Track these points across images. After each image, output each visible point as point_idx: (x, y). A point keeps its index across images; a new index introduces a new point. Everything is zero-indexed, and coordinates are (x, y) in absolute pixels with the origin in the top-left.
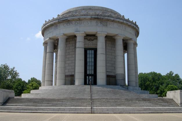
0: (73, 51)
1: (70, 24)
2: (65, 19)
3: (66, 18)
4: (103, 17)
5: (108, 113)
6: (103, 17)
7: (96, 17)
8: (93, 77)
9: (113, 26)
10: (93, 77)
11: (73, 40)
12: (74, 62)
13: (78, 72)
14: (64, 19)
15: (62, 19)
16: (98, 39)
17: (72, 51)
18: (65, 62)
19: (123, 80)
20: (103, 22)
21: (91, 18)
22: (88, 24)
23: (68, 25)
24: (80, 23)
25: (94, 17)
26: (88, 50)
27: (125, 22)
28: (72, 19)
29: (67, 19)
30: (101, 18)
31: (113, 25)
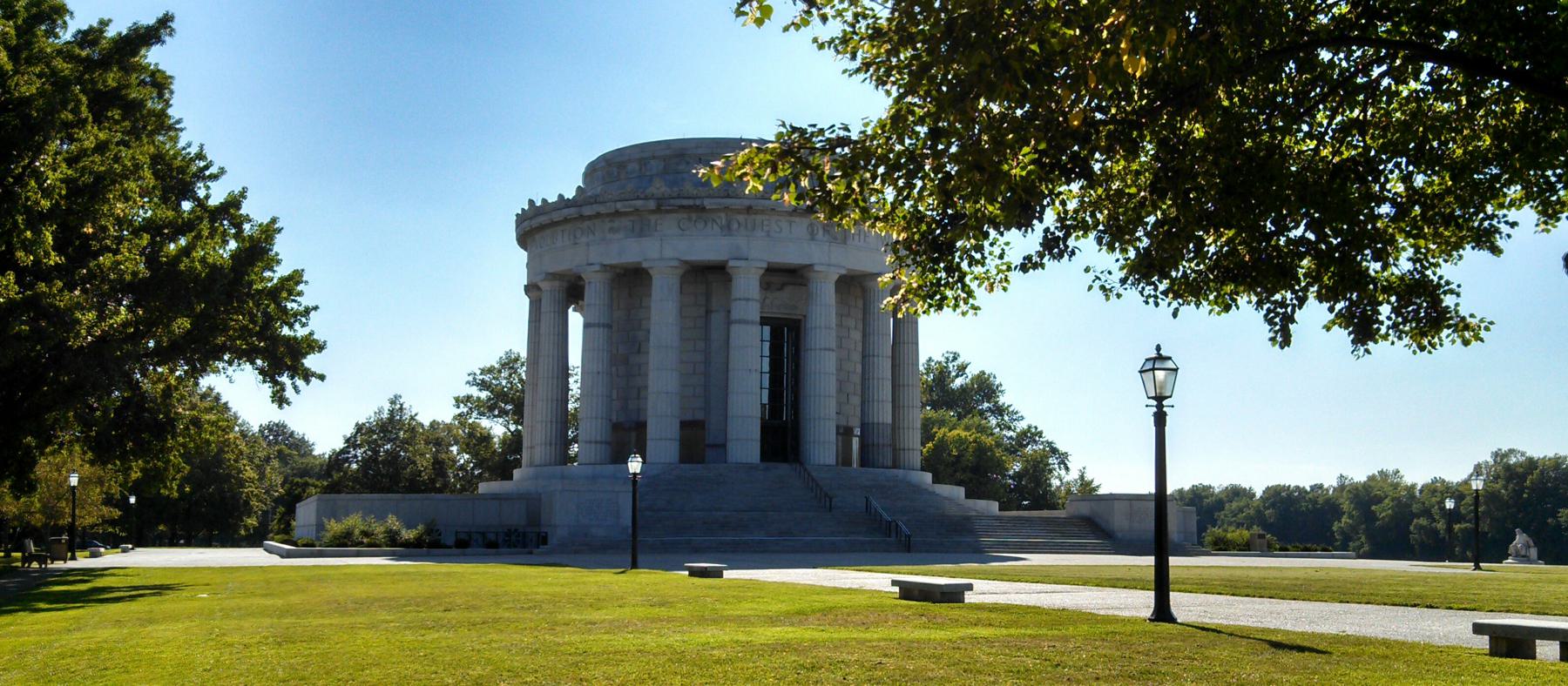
1: (709, 225)
2: (691, 202)
9: (865, 241)
14: (685, 202)
23: (701, 225)
29: (698, 202)
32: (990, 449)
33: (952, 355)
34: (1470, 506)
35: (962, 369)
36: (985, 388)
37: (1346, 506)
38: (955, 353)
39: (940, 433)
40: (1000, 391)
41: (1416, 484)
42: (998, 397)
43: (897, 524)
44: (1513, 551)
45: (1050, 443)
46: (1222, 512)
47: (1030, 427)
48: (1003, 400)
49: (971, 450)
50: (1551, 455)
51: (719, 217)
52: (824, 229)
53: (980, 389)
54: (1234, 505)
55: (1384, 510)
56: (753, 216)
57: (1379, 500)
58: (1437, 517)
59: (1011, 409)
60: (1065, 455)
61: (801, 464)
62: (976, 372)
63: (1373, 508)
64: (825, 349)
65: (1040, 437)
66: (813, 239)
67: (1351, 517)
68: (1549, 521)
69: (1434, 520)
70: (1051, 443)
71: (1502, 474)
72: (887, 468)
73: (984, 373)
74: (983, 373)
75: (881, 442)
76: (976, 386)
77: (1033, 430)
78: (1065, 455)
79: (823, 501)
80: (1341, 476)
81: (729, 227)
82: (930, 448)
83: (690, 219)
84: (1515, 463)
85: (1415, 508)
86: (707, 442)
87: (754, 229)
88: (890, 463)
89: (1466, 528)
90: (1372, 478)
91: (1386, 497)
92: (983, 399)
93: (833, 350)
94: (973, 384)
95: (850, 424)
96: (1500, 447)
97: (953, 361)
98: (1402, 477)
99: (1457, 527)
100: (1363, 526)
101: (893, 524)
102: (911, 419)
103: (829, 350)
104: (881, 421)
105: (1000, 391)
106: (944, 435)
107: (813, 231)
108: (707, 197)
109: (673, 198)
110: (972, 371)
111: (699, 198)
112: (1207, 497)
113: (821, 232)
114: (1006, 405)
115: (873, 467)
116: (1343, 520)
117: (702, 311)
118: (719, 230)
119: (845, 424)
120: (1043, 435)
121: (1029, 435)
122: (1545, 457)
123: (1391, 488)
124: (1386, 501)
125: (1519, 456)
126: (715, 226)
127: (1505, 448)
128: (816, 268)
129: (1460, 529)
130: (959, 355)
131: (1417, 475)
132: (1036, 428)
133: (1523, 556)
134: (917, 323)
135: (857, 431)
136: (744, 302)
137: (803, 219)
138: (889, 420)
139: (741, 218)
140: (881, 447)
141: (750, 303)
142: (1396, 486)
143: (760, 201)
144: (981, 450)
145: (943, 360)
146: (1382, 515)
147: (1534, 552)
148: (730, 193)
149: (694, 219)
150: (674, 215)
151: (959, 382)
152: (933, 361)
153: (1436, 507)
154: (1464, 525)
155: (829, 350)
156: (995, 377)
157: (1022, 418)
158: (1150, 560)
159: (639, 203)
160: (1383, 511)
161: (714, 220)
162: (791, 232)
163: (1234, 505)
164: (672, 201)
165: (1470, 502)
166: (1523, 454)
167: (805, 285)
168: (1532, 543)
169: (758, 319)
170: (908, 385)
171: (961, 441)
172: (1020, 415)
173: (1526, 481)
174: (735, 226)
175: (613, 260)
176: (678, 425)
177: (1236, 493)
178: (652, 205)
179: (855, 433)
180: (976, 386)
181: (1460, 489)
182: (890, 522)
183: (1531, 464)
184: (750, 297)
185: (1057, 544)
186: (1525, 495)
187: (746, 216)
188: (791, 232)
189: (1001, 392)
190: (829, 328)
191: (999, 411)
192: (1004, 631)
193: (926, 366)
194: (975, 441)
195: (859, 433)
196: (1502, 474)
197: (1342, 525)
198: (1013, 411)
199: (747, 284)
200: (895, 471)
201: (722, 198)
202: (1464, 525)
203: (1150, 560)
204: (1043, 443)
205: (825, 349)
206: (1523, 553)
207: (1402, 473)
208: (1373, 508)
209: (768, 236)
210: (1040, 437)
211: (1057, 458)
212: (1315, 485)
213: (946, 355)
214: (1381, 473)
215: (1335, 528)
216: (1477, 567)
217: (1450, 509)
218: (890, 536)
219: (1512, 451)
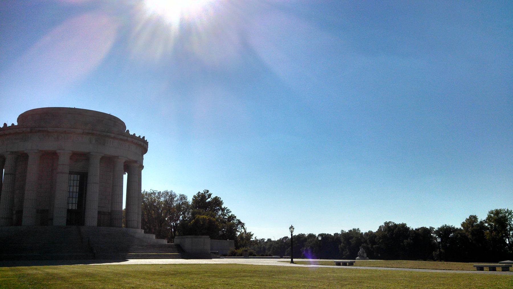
29: (46, 129)
32: (214, 222)
33: (206, 191)
34: (378, 239)
35: (210, 195)
36: (217, 202)
37: (342, 240)
38: (207, 190)
39: (197, 216)
41: (363, 233)
44: (359, 255)
45: (239, 220)
46: (306, 242)
49: (207, 222)
50: (401, 223)
53: (216, 202)
54: (309, 240)
55: (353, 241)
57: (352, 238)
58: (368, 243)
59: (227, 209)
60: (244, 224)
63: (350, 240)
65: (235, 218)
67: (344, 243)
68: (401, 244)
69: (368, 244)
70: (239, 220)
71: (387, 229)
74: (217, 197)
78: (244, 224)
80: (342, 230)
82: (193, 221)
84: (391, 226)
85: (362, 241)
89: (377, 247)
90: (350, 231)
91: (354, 237)
93: (97, 183)
96: (386, 221)
97: (207, 193)
98: (360, 230)
99: (374, 246)
100: (348, 246)
106: (199, 217)
110: (213, 196)
112: (302, 238)
114: (225, 208)
116: (341, 244)
120: (236, 218)
122: (400, 224)
123: (355, 234)
124: (354, 238)
125: (392, 223)
127: (388, 221)
129: (375, 247)
130: (209, 191)
131: (364, 230)
132: (234, 215)
133: (362, 256)
142: (357, 233)
144: (210, 222)
145: (203, 192)
146: (353, 243)
147: (365, 255)
151: (209, 200)
152: (200, 193)
153: (368, 240)
154: (376, 246)
156: (220, 198)
157: (231, 212)
158: (290, 259)
159: (24, 129)
160: (353, 241)
163: (309, 240)
165: (378, 238)
166: (394, 223)
168: (364, 251)
169: (68, 172)
171: (204, 219)
172: (230, 211)
173: (394, 231)
175: (15, 150)
177: (311, 236)
178: (29, 130)
181: (375, 234)
183: (396, 226)
185: (159, 255)
186: (394, 236)
192: (508, 264)
193: (198, 195)
194: (208, 219)
196: (387, 229)
197: (341, 246)
198: (228, 209)
199: (64, 160)
202: (376, 246)
203: (290, 259)
204: (236, 220)
206: (362, 255)
207: (360, 229)
208: (350, 240)
210: (235, 218)
211: (241, 225)
212: (336, 233)
213: (205, 191)
214: (354, 229)
215: (339, 247)
216: (292, 262)
217: (320, 240)
219: (390, 222)
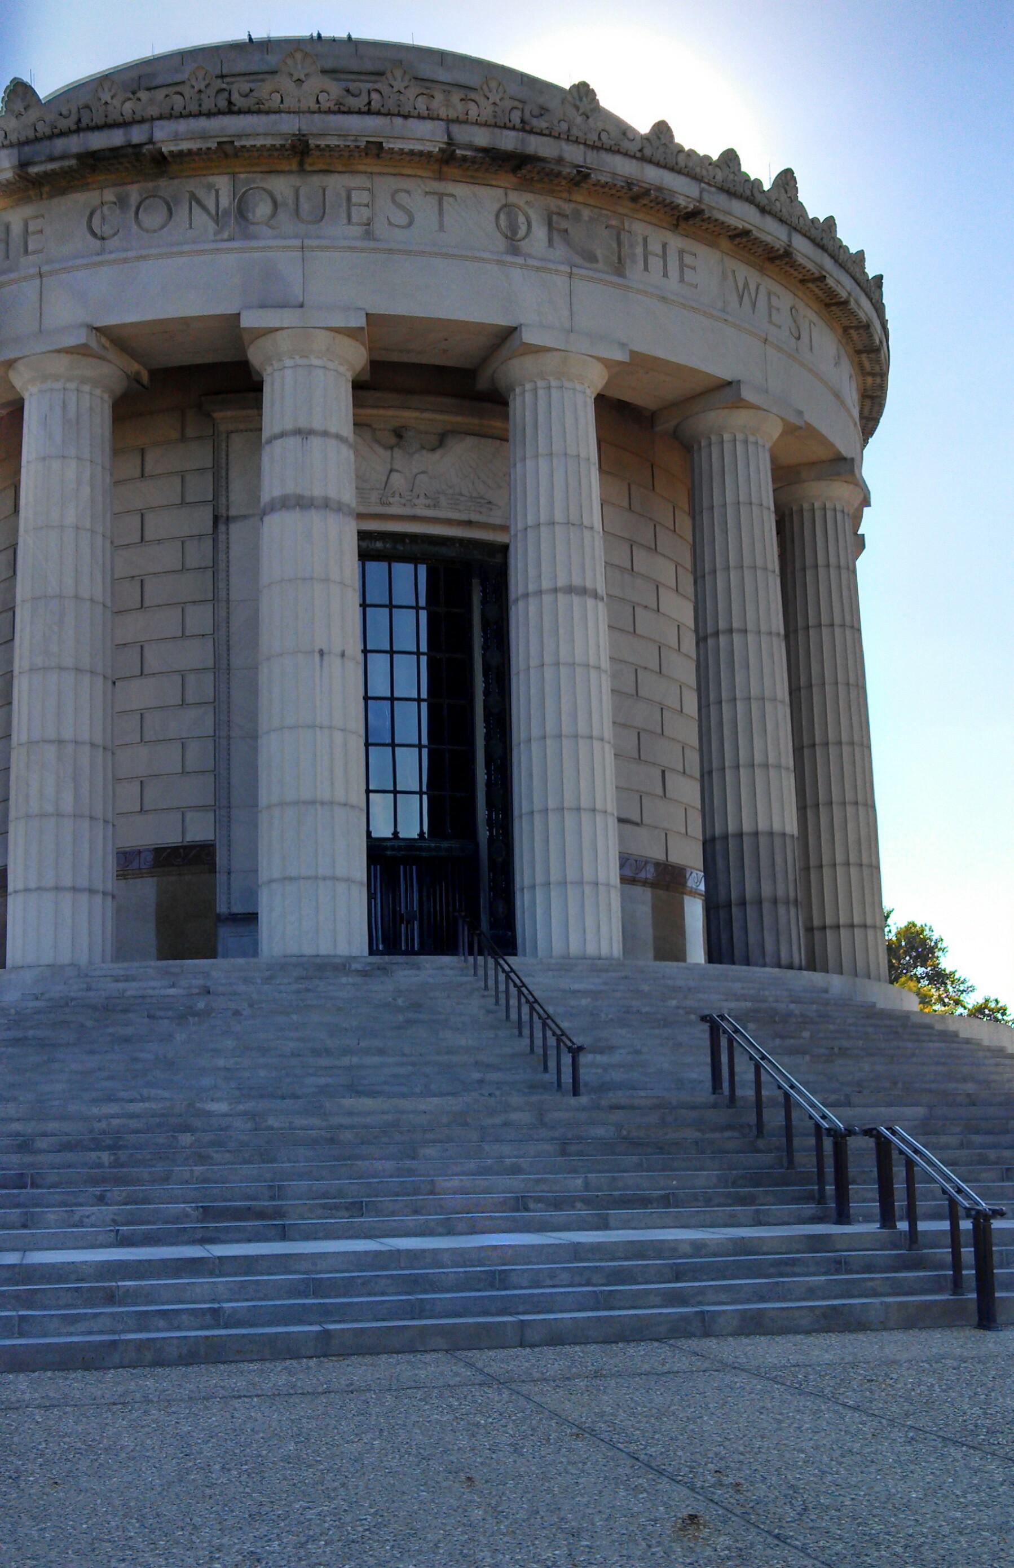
0: (192, 562)
1: (182, 213)
2: (116, 138)
3: (124, 124)
4: (592, 158)
5: (678, 1279)
6: (592, 158)
7: (508, 141)
8: (414, 868)
9: (682, 280)
10: (378, 867)
11: (190, 432)
12: (209, 693)
13: (730, 631)
14: (98, 141)
15: (75, 144)
16: (521, 405)
17: (184, 569)
18: (357, 340)
19: (233, 512)
20: (577, 216)
21: (451, 142)
22: (402, 219)
23: (153, 218)
24: (305, 206)
25: (482, 138)
26: (216, 460)
27: (801, 246)
28: (204, 137)
29: (137, 135)
30: (560, 160)
31: (682, 266)
40: (940, 949)
42: (937, 957)
43: (883, 1148)
47: (987, 1001)
48: (946, 963)
51: (210, 187)
52: (550, 224)
56: (316, 180)
61: (975, 1328)
62: (902, 924)
64: (570, 590)
65: (1003, 1014)
66: (514, 250)
72: (790, 967)
73: (914, 925)
75: (766, 891)
76: (903, 944)
77: (992, 1005)
79: (552, 1064)
81: (242, 211)
83: (122, 202)
86: (222, 908)
87: (321, 217)
88: (799, 956)
92: (915, 963)
94: (899, 940)
95: (674, 858)
101: (860, 1145)
102: (852, 837)
103: (583, 591)
104: (762, 826)
105: (940, 949)
107: (514, 228)
108: (161, 118)
109: (62, 134)
111: (142, 121)
113: (540, 232)
115: (748, 963)
117: (205, 515)
118: (211, 226)
119: (660, 856)
120: (1008, 1012)
121: (987, 1011)
126: (196, 210)
128: (529, 337)
132: (997, 1001)
134: (854, 571)
135: (696, 881)
136: (292, 442)
137: (483, 191)
138: (792, 827)
139: (282, 186)
140: (766, 906)
141: (316, 442)
143: (332, 118)
148: (236, 97)
149: (134, 199)
150: (80, 200)
155: (583, 591)
156: (931, 930)
161: (194, 197)
162: (441, 228)
164: (60, 145)
167: (507, 440)
170: (840, 743)
174: (262, 209)
176: (111, 861)
179: (691, 883)
180: (903, 944)
182: (839, 1138)
184: (317, 425)
187: (295, 180)
188: (441, 228)
189: (943, 950)
190: (581, 526)
191: (939, 977)
195: (702, 887)
200: (817, 978)
201: (209, 115)
205: (570, 590)
209: (369, 234)
210: (1003, 1014)
218: (843, 1217)
